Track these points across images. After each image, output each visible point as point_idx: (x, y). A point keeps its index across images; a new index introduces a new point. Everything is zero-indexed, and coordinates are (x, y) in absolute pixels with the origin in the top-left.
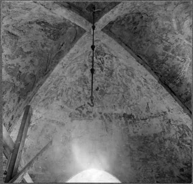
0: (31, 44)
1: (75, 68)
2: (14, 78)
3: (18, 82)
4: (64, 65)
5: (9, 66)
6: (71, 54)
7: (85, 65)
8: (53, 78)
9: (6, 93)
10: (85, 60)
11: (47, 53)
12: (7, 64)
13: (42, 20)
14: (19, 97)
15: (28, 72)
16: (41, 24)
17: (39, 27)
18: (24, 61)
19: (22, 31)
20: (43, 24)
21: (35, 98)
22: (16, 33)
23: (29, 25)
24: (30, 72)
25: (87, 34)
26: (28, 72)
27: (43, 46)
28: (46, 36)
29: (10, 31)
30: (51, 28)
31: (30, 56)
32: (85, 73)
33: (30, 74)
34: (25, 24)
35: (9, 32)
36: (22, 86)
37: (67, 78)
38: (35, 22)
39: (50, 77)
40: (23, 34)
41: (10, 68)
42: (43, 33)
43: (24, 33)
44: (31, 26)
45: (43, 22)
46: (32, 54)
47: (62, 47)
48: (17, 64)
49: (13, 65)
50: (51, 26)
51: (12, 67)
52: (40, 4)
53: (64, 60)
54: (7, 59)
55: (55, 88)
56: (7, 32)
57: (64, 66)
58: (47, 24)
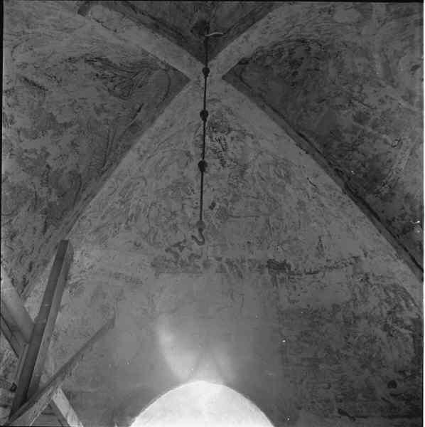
0: (71, 105)
1: (165, 159)
2: (36, 180)
3: (45, 189)
4: (142, 153)
5: (25, 154)
6: (157, 129)
7: (188, 154)
8: (119, 181)
9: (17, 214)
10: (186, 144)
11: (107, 127)
12: (21, 148)
13: (98, 55)
14: (46, 222)
15: (66, 168)
16: (95, 63)
17: (90, 68)
18: (57, 143)
19: (54, 78)
20: (99, 63)
21: (79, 225)
22: (40, 81)
23: (68, 64)
24: (69, 169)
25: (191, 87)
26: (66, 168)
27: (98, 112)
28: (104, 89)
29: (29, 78)
30: (117, 73)
31: (71, 133)
32: (186, 171)
33: (70, 172)
34: (62, 63)
35: (26, 79)
36: (54, 198)
37: (149, 181)
38: (82, 57)
39: (113, 179)
40: (56, 83)
41: (27, 157)
42: (99, 82)
43: (58, 82)
44: (74, 67)
45: (99, 59)
46: (74, 127)
47: (139, 114)
48: (43, 149)
49: (35, 151)
50: (115, 67)
51: (33, 156)
52: (94, 19)
53: (143, 143)
54: (22, 137)
55: (123, 203)
56: (23, 79)
57: (141, 156)
58: (107, 64)
